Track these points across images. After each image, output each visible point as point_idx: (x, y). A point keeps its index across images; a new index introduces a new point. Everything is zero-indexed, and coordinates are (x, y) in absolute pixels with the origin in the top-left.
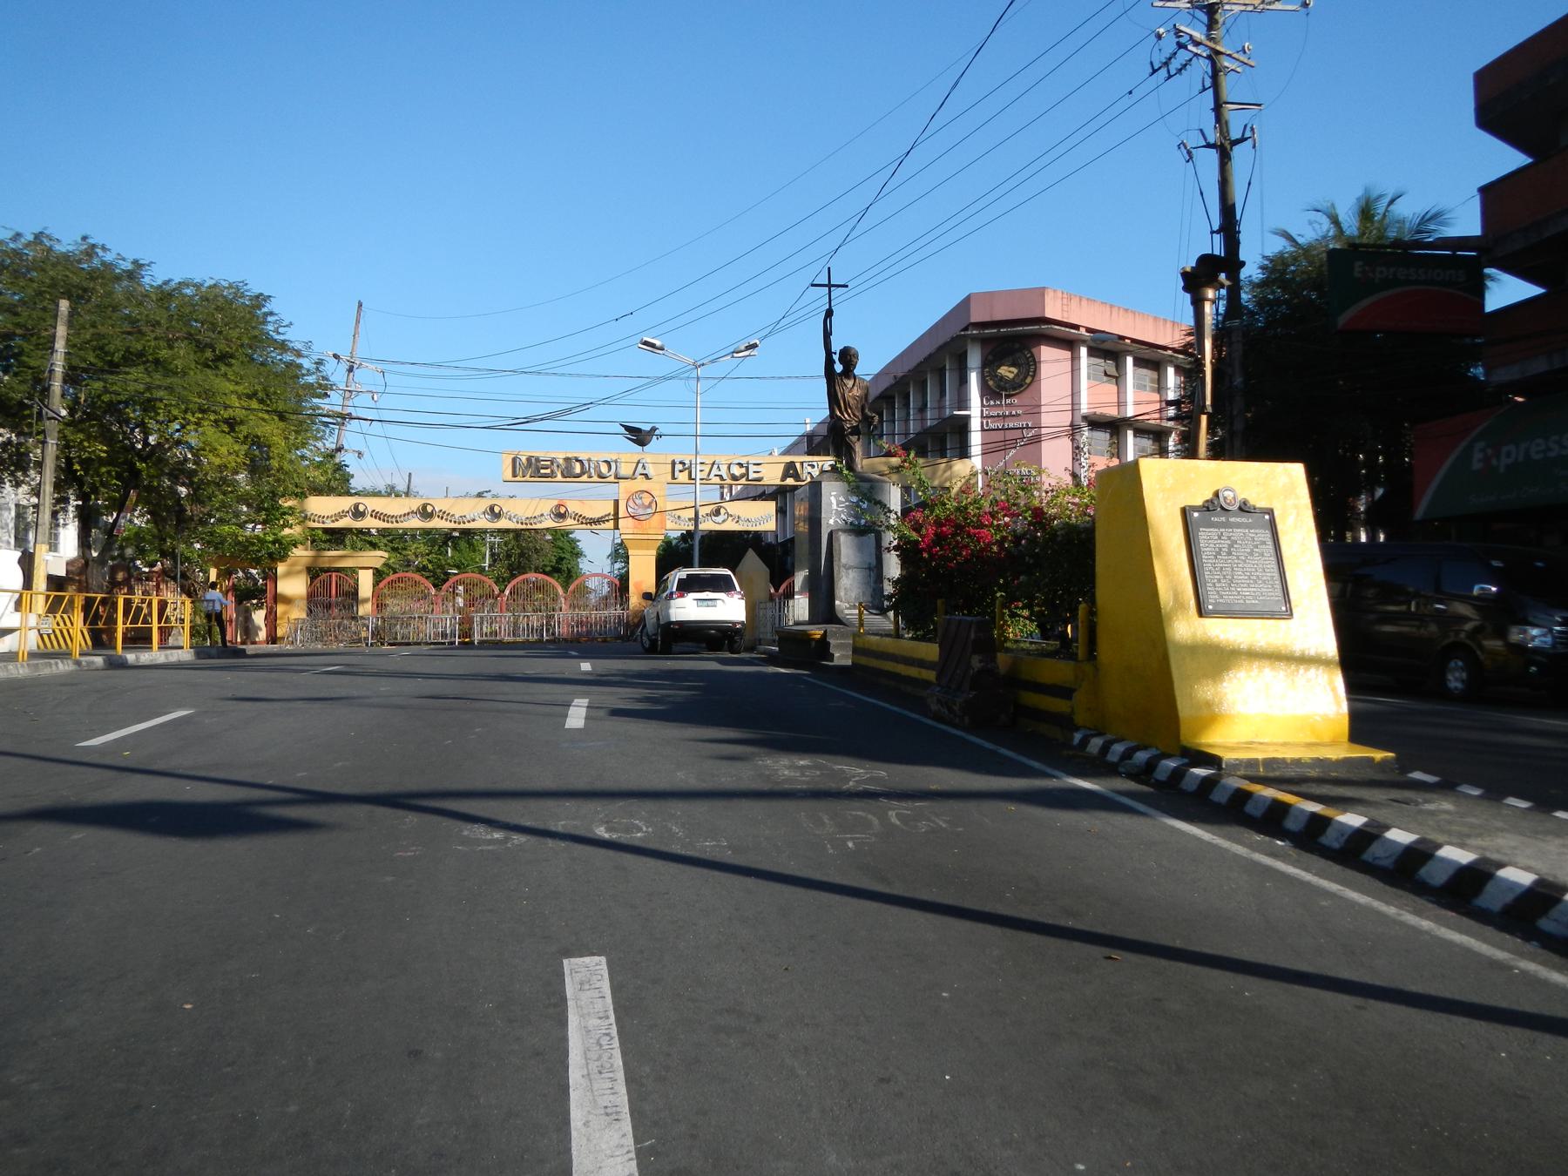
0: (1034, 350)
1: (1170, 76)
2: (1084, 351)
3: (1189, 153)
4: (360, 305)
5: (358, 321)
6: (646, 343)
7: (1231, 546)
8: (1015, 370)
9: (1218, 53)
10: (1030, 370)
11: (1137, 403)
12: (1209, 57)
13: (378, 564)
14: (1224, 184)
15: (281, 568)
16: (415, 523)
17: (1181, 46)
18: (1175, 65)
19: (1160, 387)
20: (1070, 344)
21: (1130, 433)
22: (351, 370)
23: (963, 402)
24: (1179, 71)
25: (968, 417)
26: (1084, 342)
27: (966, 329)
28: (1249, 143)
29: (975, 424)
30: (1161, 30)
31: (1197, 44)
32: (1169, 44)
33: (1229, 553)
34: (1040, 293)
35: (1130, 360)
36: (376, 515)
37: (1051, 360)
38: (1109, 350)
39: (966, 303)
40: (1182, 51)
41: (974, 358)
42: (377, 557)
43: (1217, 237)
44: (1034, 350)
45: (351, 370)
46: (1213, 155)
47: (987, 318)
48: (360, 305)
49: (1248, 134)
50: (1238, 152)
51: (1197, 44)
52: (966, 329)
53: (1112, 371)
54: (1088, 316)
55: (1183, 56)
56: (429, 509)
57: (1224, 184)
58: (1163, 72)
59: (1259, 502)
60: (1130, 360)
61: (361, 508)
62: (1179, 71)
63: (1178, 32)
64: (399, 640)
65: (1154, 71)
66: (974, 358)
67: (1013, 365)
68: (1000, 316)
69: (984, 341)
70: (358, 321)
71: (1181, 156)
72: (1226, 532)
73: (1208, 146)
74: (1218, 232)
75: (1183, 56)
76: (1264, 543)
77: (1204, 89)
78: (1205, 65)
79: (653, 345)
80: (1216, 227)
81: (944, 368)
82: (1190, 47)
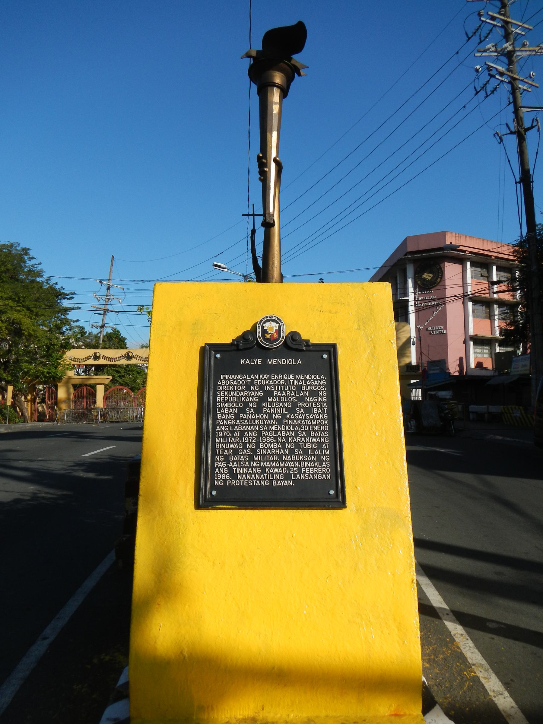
0: (442, 265)
1: (487, 96)
2: (468, 264)
3: (501, 138)
4: (113, 257)
5: (112, 265)
6: (216, 265)
7: (262, 399)
8: (431, 275)
9: (515, 79)
10: (439, 274)
11: (473, 284)
12: (509, 82)
13: (107, 382)
14: (522, 153)
15: (59, 384)
16: (124, 362)
17: (492, 76)
18: (489, 88)
19: (489, 276)
20: (460, 260)
21: (496, 306)
22: (108, 288)
23: (406, 294)
24: (493, 92)
25: (407, 301)
26: (468, 259)
27: (406, 255)
28: (536, 128)
29: (411, 303)
30: (478, 67)
31: (501, 74)
32: (485, 77)
33: (258, 410)
34: (443, 234)
35: (494, 268)
36: (105, 358)
37: (451, 271)
38: (482, 262)
39: (405, 243)
40: (492, 79)
41: (410, 270)
42: (106, 378)
43: (518, 185)
44: (442, 265)
45: (108, 288)
46: (514, 137)
47: (416, 249)
48: (113, 257)
49: (535, 124)
50: (530, 136)
51: (501, 74)
52: (406, 255)
53: (485, 274)
54: (470, 244)
55: (493, 82)
56: (130, 354)
57: (522, 153)
58: (482, 94)
59: (313, 333)
60: (494, 268)
61: (98, 354)
62: (493, 92)
63: (489, 68)
64: (114, 419)
65: (477, 93)
66: (410, 270)
67: (430, 273)
68: (423, 247)
69: (414, 261)
70: (112, 265)
71: (495, 141)
72: (264, 379)
73: (512, 133)
74: (519, 182)
75: (493, 82)
76: (314, 394)
77: (510, 103)
78: (508, 87)
79: (220, 266)
80: (518, 180)
81: (396, 277)
82: (497, 76)
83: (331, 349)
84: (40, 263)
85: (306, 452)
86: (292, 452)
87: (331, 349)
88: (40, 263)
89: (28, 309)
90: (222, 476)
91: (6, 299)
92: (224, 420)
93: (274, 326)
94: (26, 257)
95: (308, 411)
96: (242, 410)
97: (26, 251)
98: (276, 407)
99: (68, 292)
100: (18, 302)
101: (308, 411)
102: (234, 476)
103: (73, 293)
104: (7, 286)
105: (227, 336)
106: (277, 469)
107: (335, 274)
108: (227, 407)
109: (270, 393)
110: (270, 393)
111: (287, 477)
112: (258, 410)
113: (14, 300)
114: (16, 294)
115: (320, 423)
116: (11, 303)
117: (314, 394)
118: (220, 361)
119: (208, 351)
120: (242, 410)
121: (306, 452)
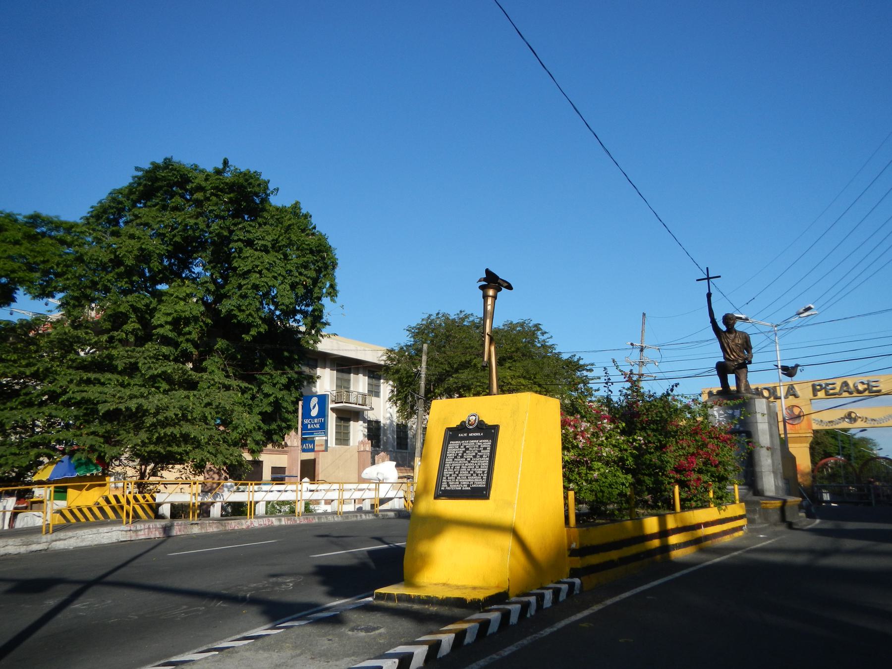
4: (644, 314)
5: (643, 323)
7: (464, 452)
22: (642, 350)
33: (462, 457)
45: (642, 350)
48: (644, 314)
59: (489, 421)
70: (643, 323)
83: (496, 428)
84: (551, 337)
85: (477, 475)
86: (472, 475)
87: (496, 428)
88: (551, 337)
89: (540, 385)
90: (444, 486)
91: (519, 377)
92: (449, 461)
93: (474, 418)
94: (539, 333)
95: (481, 456)
96: (456, 457)
97: (537, 327)
98: (469, 455)
99: (587, 363)
100: (530, 379)
101: (481, 456)
102: (449, 486)
103: (592, 364)
104: (518, 364)
105: (455, 423)
106: (465, 482)
107: (861, 318)
108: (451, 454)
109: (468, 449)
110: (468, 449)
111: (468, 486)
112: (462, 457)
113: (524, 378)
114: (527, 372)
115: (485, 462)
116: (522, 381)
117: (485, 449)
118: (454, 434)
119: (449, 429)
120: (456, 457)
121: (477, 475)
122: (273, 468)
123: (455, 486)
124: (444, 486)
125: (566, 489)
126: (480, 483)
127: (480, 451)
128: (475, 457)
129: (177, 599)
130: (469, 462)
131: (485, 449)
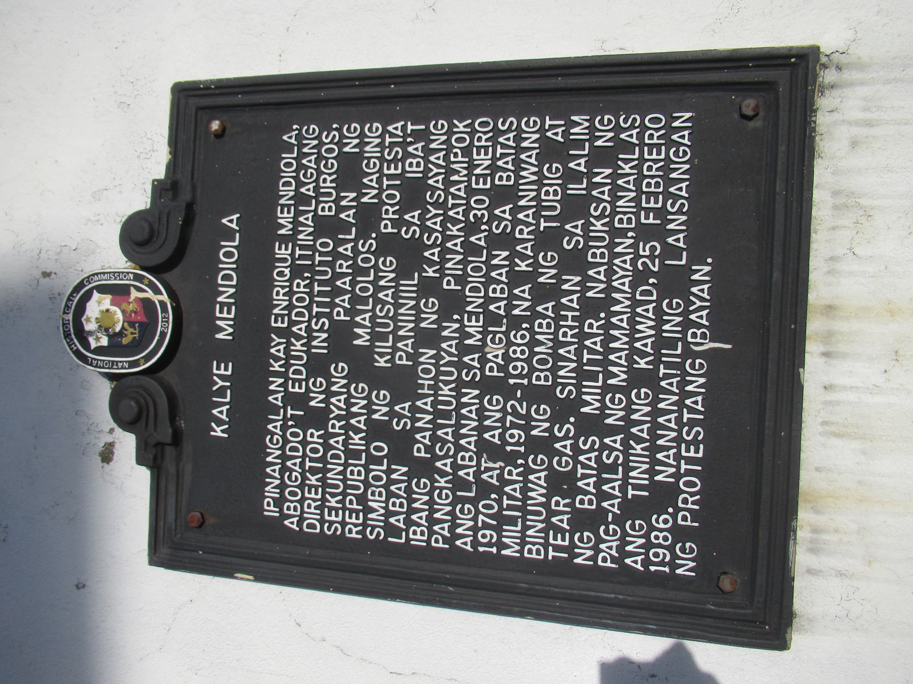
7: (362, 368)
33: (401, 382)
85: (575, 207)
92: (432, 520)
95: (413, 193)
98: (391, 314)
101: (413, 193)
102: (662, 497)
106: (635, 323)
109: (341, 334)
110: (341, 334)
111: (674, 284)
121: (575, 207)
122: (185, 94)
123: (672, 446)
124: (660, 548)
125: (236, 578)
126: (662, 148)
127: (368, 217)
128: (409, 255)
129: (132, 377)
130: (452, 305)
131: (350, 172)
